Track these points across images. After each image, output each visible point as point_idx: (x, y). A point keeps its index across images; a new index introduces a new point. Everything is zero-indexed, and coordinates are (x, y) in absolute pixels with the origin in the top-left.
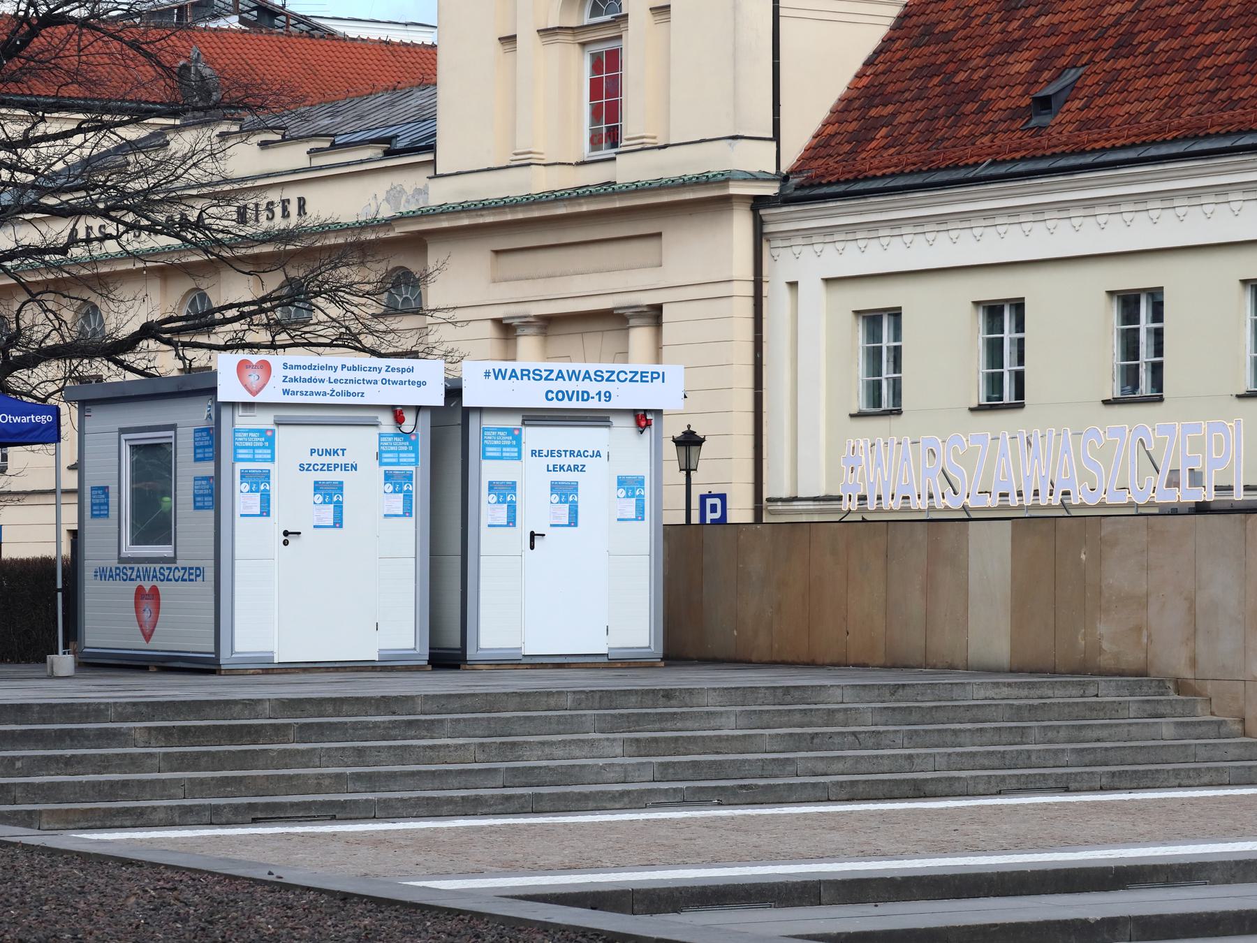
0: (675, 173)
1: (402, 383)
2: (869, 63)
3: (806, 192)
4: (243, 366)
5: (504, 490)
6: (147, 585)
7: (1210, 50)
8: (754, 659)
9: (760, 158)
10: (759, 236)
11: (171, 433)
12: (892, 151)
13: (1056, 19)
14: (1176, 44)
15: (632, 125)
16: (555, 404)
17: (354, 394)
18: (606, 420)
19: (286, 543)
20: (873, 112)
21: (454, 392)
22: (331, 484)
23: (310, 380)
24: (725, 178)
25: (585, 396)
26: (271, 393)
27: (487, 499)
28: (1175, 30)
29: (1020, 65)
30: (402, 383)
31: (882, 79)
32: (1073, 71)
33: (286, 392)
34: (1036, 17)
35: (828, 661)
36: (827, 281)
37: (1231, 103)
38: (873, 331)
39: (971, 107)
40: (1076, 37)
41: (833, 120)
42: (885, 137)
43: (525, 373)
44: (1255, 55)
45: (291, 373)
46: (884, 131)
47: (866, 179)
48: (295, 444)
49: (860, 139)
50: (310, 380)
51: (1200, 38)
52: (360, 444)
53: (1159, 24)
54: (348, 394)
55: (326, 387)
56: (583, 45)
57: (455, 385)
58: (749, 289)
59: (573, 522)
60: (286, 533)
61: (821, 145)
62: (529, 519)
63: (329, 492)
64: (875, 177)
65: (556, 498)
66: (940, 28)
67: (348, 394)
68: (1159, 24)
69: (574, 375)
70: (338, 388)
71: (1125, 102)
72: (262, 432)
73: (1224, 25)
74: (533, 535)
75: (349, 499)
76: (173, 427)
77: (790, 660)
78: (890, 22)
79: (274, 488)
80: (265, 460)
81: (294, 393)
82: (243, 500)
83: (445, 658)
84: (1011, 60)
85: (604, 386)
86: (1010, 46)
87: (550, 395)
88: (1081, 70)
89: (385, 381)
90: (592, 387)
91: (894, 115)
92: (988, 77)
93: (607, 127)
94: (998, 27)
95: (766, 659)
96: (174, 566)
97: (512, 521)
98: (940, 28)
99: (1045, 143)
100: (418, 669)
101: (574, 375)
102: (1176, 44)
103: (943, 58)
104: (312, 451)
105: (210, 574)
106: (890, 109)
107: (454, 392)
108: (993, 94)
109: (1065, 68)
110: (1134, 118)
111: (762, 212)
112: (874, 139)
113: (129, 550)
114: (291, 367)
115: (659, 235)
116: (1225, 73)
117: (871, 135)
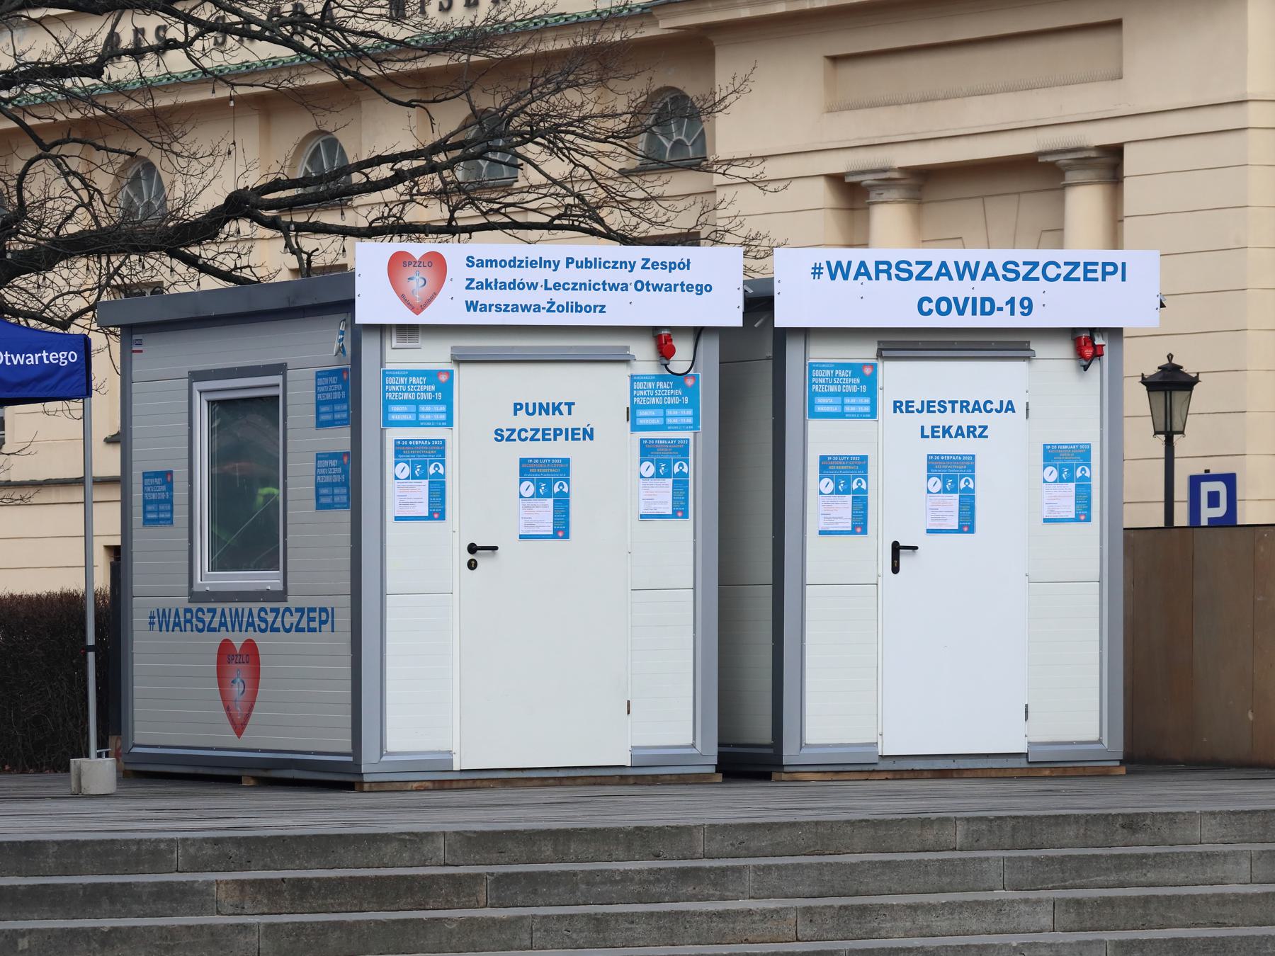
4: (398, 263)
11: (278, 379)
17: (589, 309)
18: (1024, 347)
19: (472, 565)
21: (759, 302)
22: (549, 463)
23: (513, 285)
25: (987, 305)
27: (818, 486)
30: (669, 288)
33: (471, 306)
45: (480, 274)
48: (485, 394)
50: (513, 285)
52: (599, 394)
54: (578, 308)
55: (540, 297)
57: (762, 291)
59: (967, 524)
60: (472, 549)
63: (546, 477)
67: (578, 308)
69: (967, 271)
70: (561, 297)
74: (896, 548)
76: (280, 369)
80: (436, 424)
81: (485, 308)
82: (401, 492)
83: (747, 759)
85: (1020, 289)
89: (641, 286)
90: (1000, 291)
104: (517, 407)
105: (343, 619)
107: (759, 302)
113: (208, 579)
114: (481, 263)
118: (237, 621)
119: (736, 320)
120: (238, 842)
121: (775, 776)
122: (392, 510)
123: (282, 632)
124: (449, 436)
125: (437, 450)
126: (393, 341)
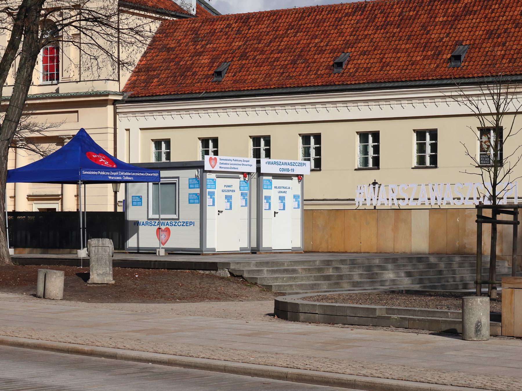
3: (133, 99)
5: (268, 198)
7: (277, 59)
8: (320, 251)
10: (115, 113)
11: (177, 179)
12: (161, 86)
14: (264, 57)
16: (282, 173)
17: (236, 168)
19: (219, 214)
22: (229, 196)
23: (226, 164)
25: (288, 170)
26: (217, 168)
27: (264, 201)
28: (262, 52)
29: (205, 60)
32: (226, 63)
33: (220, 167)
36: (141, 129)
37: (289, 77)
40: (225, 52)
43: (275, 163)
46: (156, 80)
47: (156, 95)
48: (221, 183)
49: (148, 81)
50: (226, 164)
52: (235, 183)
53: (256, 50)
54: (234, 168)
55: (229, 166)
58: (112, 131)
59: (284, 209)
60: (219, 211)
62: (274, 209)
63: (228, 198)
64: (160, 95)
65: (226, 201)
67: (234, 168)
68: (256, 50)
69: (286, 164)
70: (232, 166)
72: (213, 180)
73: (281, 52)
75: (233, 200)
76: (178, 178)
77: (336, 251)
79: (216, 197)
80: (213, 188)
82: (209, 201)
84: (201, 58)
85: (292, 167)
86: (200, 54)
88: (229, 63)
89: (243, 165)
95: (343, 251)
96: (177, 221)
97: (270, 209)
100: (301, 253)
101: (286, 164)
102: (264, 57)
104: (225, 186)
110: (254, 81)
112: (152, 82)
113: (151, 216)
114: (222, 160)
116: (285, 67)
120: (293, 262)
122: (208, 204)
124: (216, 191)
125: (213, 193)
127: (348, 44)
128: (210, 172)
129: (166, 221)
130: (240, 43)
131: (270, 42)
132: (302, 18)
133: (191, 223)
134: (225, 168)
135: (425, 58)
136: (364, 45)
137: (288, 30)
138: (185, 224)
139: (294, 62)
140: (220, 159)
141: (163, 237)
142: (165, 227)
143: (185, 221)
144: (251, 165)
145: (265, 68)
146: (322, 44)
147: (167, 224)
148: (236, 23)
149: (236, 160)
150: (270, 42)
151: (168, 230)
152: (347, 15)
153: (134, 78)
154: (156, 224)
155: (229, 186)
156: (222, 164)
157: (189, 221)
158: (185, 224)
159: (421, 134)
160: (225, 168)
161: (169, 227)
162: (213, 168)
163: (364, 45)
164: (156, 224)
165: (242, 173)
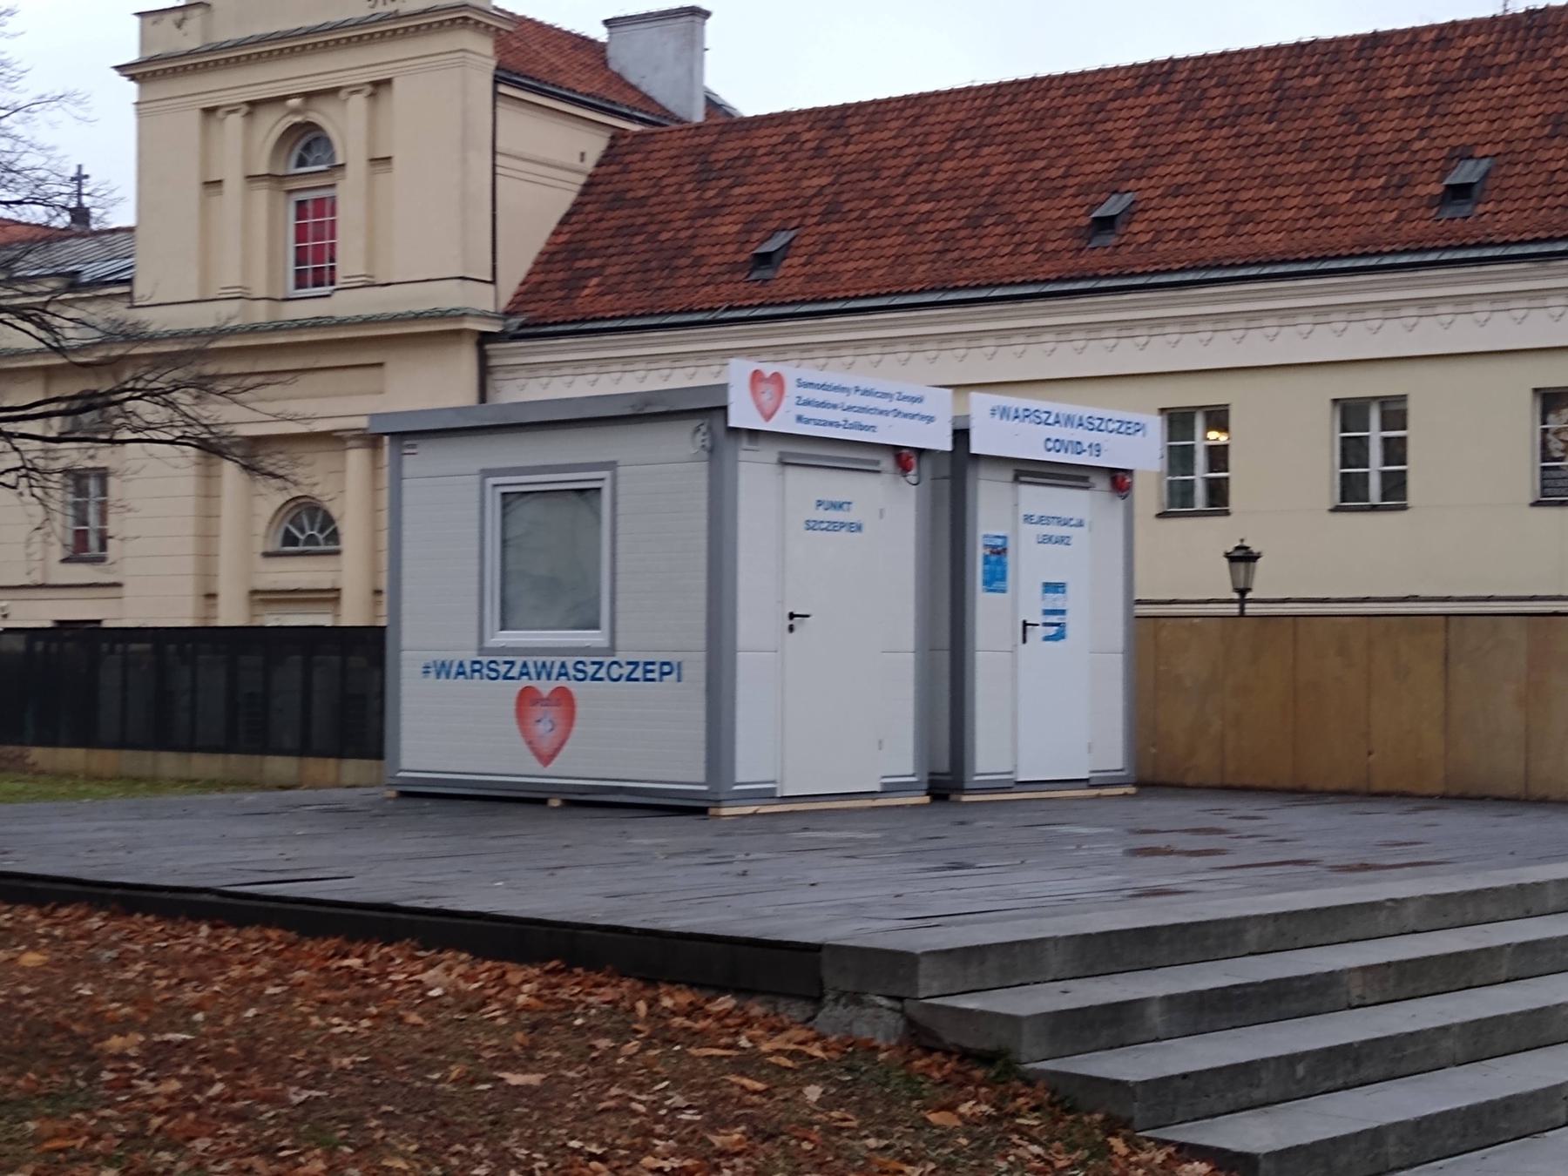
0: (367, 312)
1: (913, 416)
2: (563, 222)
4: (756, 376)
6: (545, 687)
9: (484, 299)
12: (609, 297)
13: (754, 189)
15: (349, 263)
18: (1085, 479)
19: (791, 629)
20: (578, 264)
21: (961, 435)
23: (823, 405)
24: (462, 315)
25: (1077, 448)
26: (783, 422)
29: (728, 226)
30: (913, 416)
31: (580, 236)
33: (799, 419)
34: (731, 187)
35: (1331, 786)
38: (81, 491)
39: (683, 262)
40: (780, 204)
41: (538, 269)
42: (598, 285)
44: (1558, 126)
45: (808, 394)
46: (595, 281)
49: (573, 285)
50: (823, 405)
51: (912, 208)
53: (866, 194)
56: (290, 192)
57: (960, 426)
61: (530, 290)
66: (630, 195)
68: (866, 194)
69: (1069, 420)
70: (853, 417)
71: (846, 261)
73: (934, 197)
74: (1025, 624)
76: (611, 466)
78: (578, 188)
81: (808, 421)
83: (945, 785)
85: (1095, 437)
86: (715, 211)
87: (1050, 445)
89: (897, 413)
90: (1087, 437)
91: (603, 267)
92: (694, 237)
93: (314, 265)
94: (694, 195)
95: (1288, 784)
98: (630, 195)
99: (774, 292)
101: (1069, 420)
103: (641, 220)
104: (820, 503)
105: (695, 670)
106: (595, 262)
107: (961, 435)
108: (704, 251)
109: (776, 230)
111: (488, 347)
115: (380, 365)
117: (583, 283)
118: (544, 671)
119: (948, 447)
121: (953, 797)
123: (607, 682)
126: (745, 443)
127: (1125, 172)
128: (754, 434)
129: (558, 660)
130: (824, 181)
131: (906, 175)
132: (992, 110)
133: (668, 669)
134: (818, 423)
135: (1363, 195)
136: (1177, 169)
137: (953, 140)
138: (638, 674)
139: (974, 222)
140: (802, 384)
141: (543, 729)
142: (553, 684)
143: (641, 658)
144: (930, 419)
145: (892, 242)
146: (1053, 173)
147: (563, 673)
148: (810, 129)
149: (866, 393)
150: (906, 175)
151: (564, 698)
152: (1120, 95)
153: (536, 278)
154: (515, 672)
155: (838, 506)
156: (808, 403)
157: (659, 657)
158: (638, 674)
159: (1351, 412)
160: (818, 423)
161: (572, 686)
162: (768, 417)
163: (1177, 169)
164: (515, 672)
165: (896, 451)
